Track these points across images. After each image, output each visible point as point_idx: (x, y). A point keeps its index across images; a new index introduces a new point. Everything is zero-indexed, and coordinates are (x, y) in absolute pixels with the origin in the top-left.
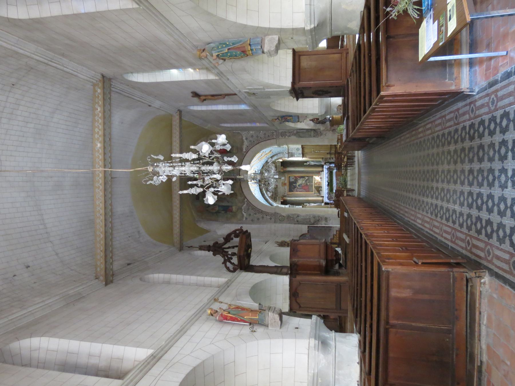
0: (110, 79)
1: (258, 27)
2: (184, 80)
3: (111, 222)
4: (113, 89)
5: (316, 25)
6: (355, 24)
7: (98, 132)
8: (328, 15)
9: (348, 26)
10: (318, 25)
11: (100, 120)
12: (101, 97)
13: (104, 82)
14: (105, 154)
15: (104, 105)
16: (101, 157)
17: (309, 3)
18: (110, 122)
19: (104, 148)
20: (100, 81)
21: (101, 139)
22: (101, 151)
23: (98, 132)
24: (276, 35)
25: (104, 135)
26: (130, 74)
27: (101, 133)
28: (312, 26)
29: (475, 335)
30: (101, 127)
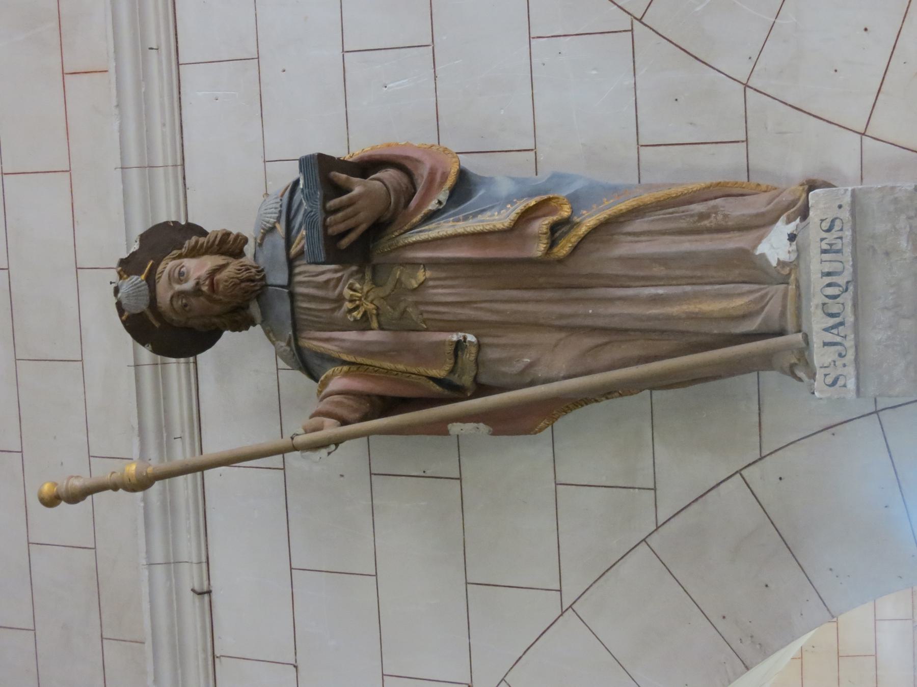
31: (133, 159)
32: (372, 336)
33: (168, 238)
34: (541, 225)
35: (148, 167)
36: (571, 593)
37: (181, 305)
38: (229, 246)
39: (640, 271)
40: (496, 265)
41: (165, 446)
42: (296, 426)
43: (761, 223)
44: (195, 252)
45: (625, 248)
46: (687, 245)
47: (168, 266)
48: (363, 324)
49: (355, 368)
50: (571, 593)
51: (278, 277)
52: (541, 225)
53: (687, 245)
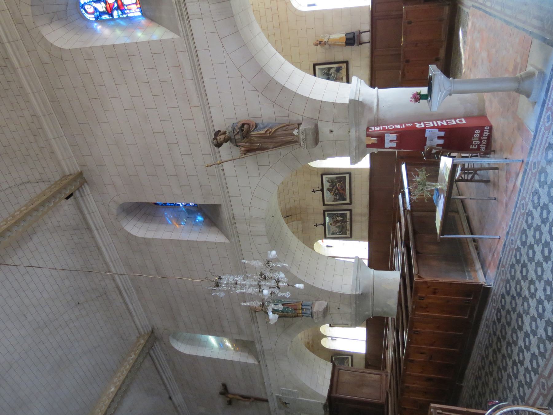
0: (156, 338)
1: (313, 286)
2: (223, 358)
3: (141, 364)
4: (151, 352)
5: (360, 293)
6: (393, 303)
7: (120, 377)
8: (371, 290)
9: (388, 303)
10: (362, 294)
11: (104, 407)
12: (141, 347)
13: (150, 337)
14: (113, 401)
15: (139, 356)
16: (108, 402)
17: (356, 278)
18: (122, 397)
19: (116, 395)
20: (148, 333)
21: (118, 384)
22: (111, 396)
23: (120, 377)
24: (325, 301)
25: (124, 382)
26: (175, 341)
27: (122, 378)
28: (358, 293)
29: (462, 63)
30: (125, 373)
31: (185, 35)
32: (247, 144)
33: (217, 133)
34: (268, 132)
35: (195, 66)
36: (271, 165)
37: (219, 140)
38: (225, 133)
39: (279, 136)
40: (262, 137)
41: (217, 160)
42: (216, 114)
43: (294, 129)
44: (221, 135)
45: (278, 133)
46: (285, 132)
47: (218, 138)
48: (246, 143)
49: (244, 147)
50: (271, 165)
51: (233, 137)
52: (268, 132)
53: (285, 132)
